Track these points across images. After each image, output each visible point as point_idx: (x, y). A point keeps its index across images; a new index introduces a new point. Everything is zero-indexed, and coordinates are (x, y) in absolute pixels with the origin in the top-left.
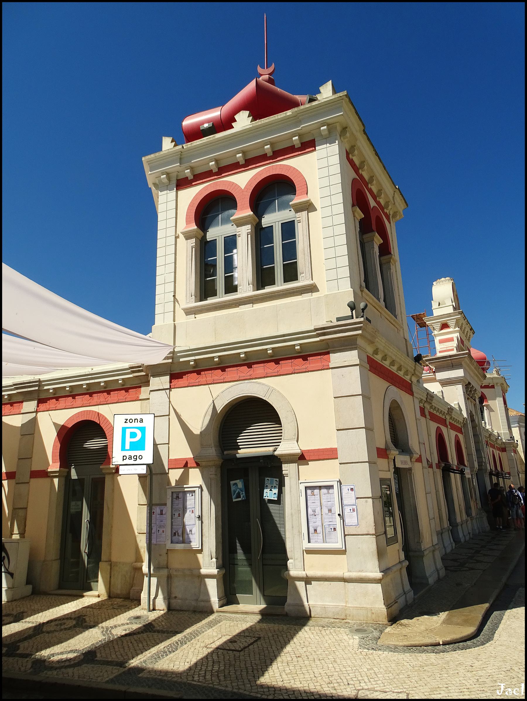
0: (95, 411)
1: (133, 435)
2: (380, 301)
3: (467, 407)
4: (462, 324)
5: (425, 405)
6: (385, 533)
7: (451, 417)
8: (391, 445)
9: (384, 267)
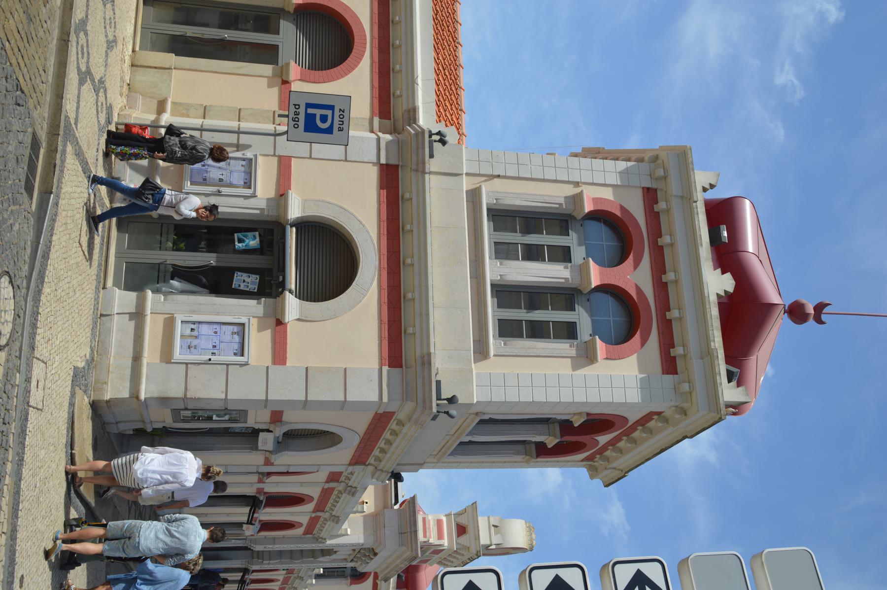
0: (364, 54)
1: (324, 119)
2: (467, 435)
3: (342, 546)
4: (463, 555)
5: (343, 485)
6: (186, 409)
7: (328, 519)
8: (285, 429)
9: (520, 447)
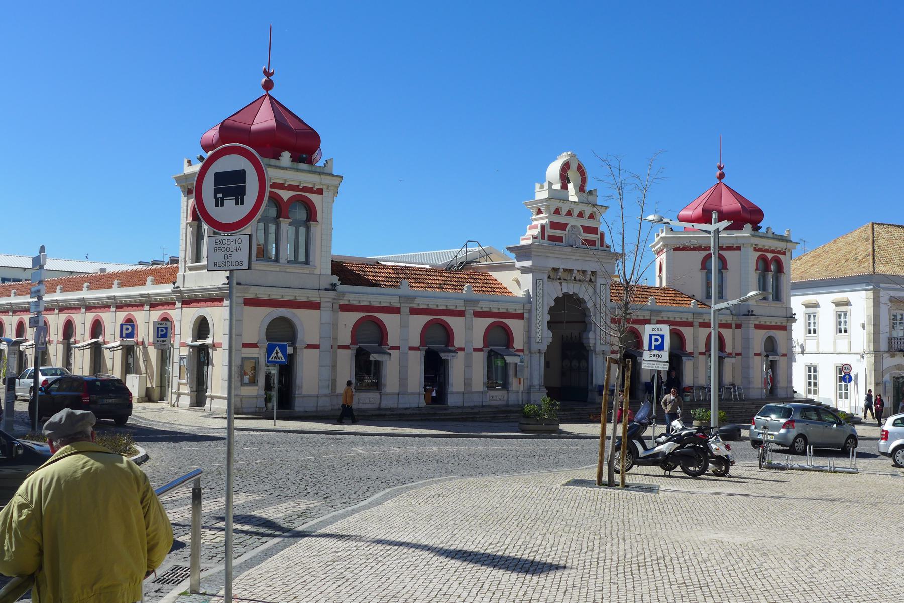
1: (162, 331)
